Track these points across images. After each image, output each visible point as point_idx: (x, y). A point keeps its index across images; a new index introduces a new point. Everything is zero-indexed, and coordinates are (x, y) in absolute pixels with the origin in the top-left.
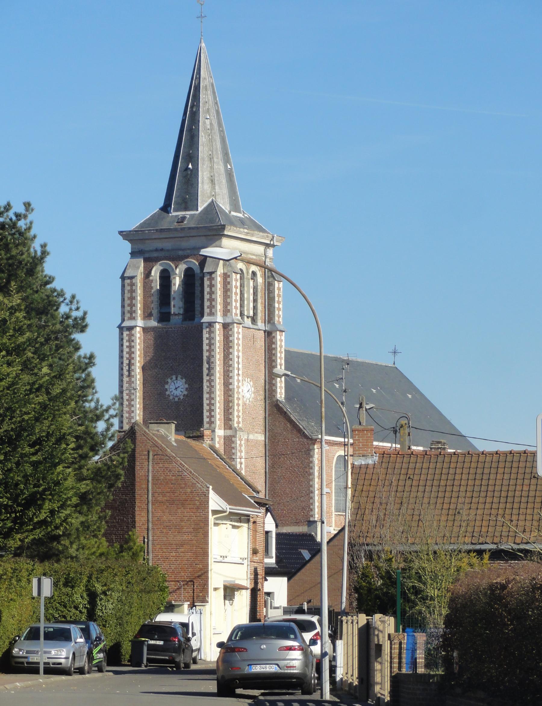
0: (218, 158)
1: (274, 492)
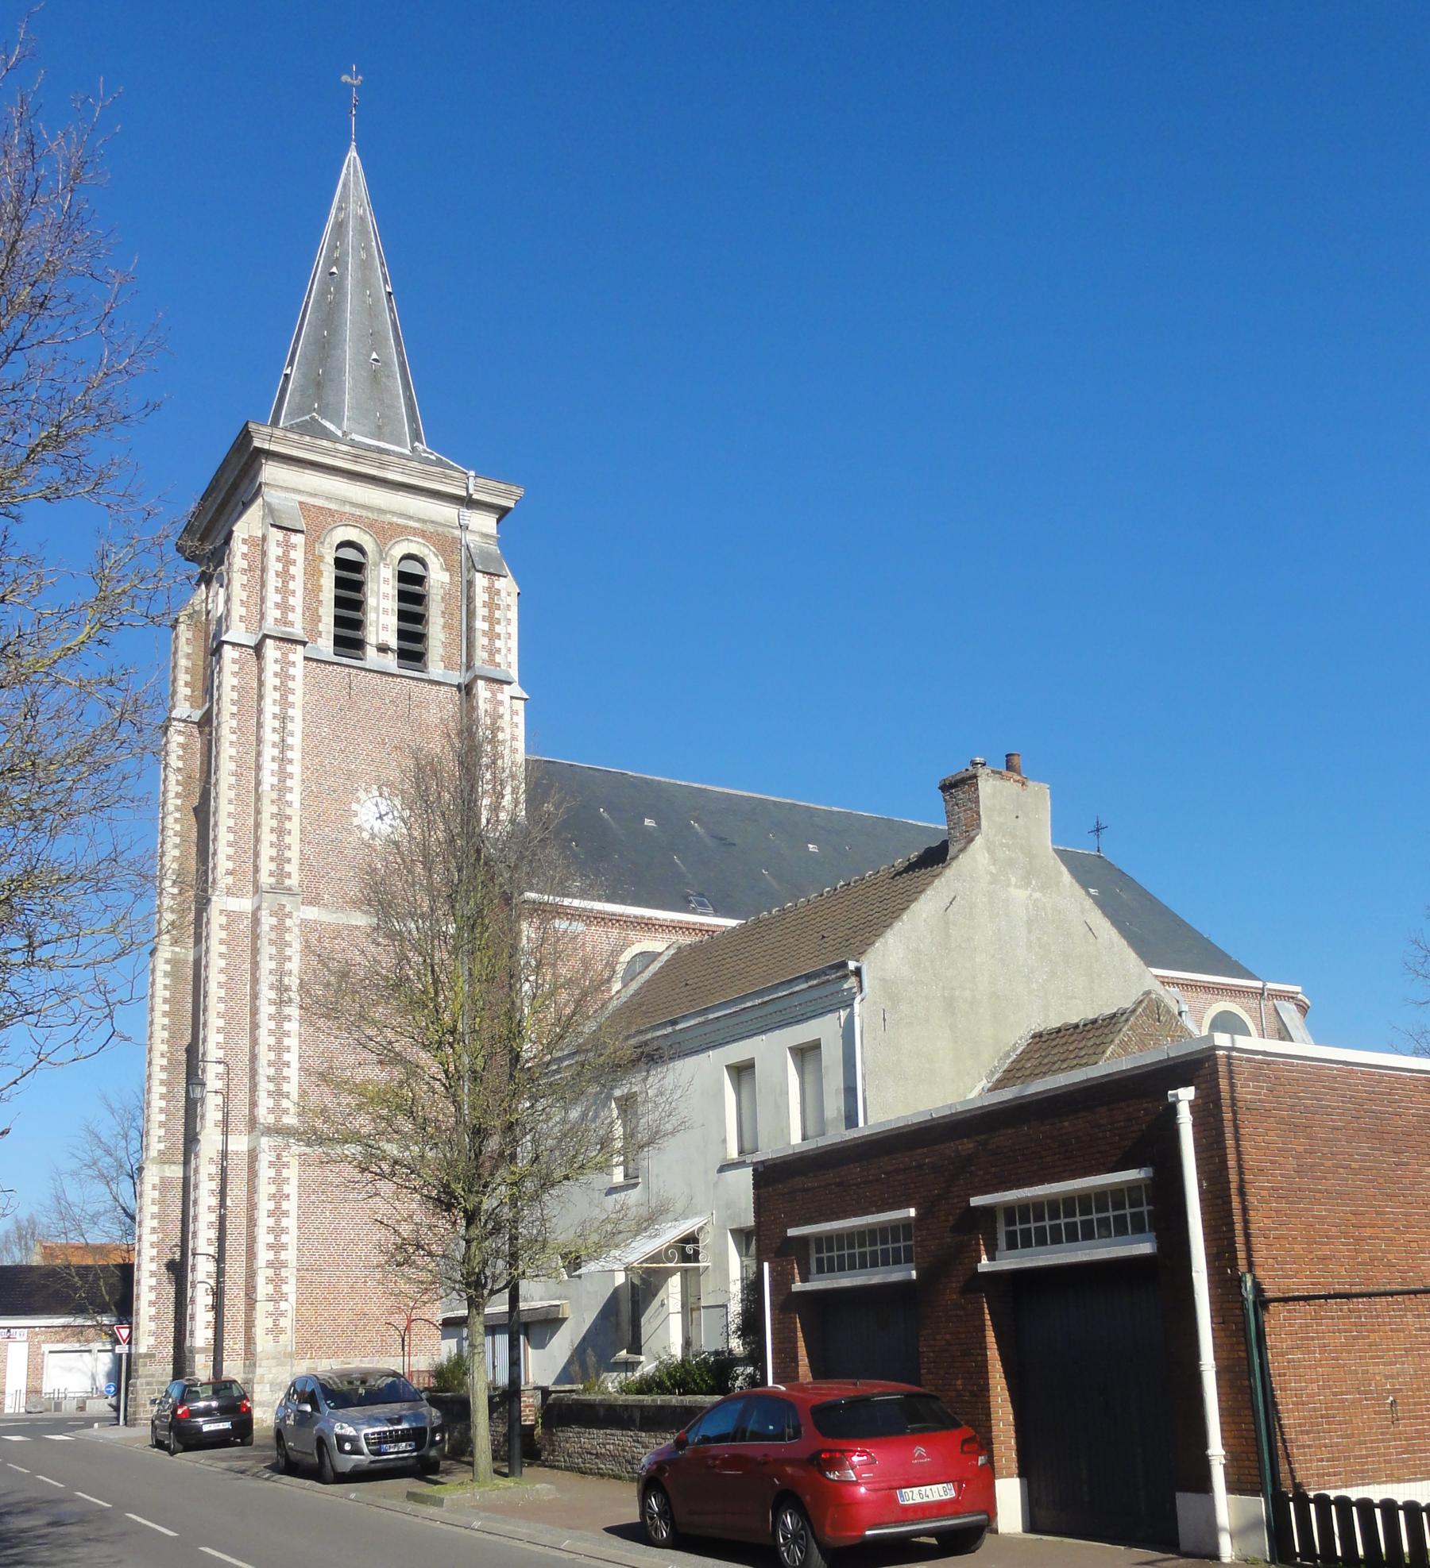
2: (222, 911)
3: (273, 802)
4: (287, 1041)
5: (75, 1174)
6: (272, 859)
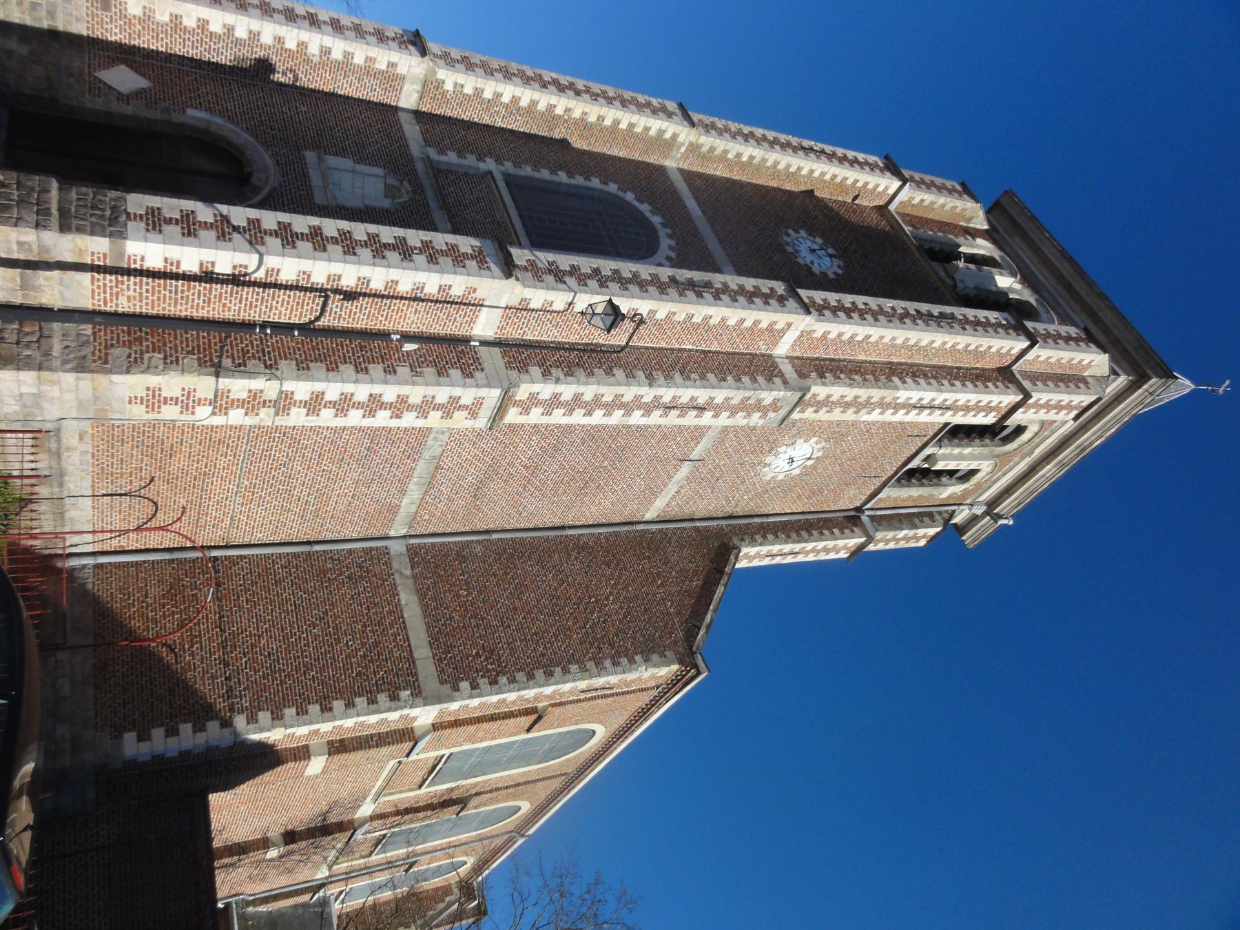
0: (471, 304)
1: (512, 555)
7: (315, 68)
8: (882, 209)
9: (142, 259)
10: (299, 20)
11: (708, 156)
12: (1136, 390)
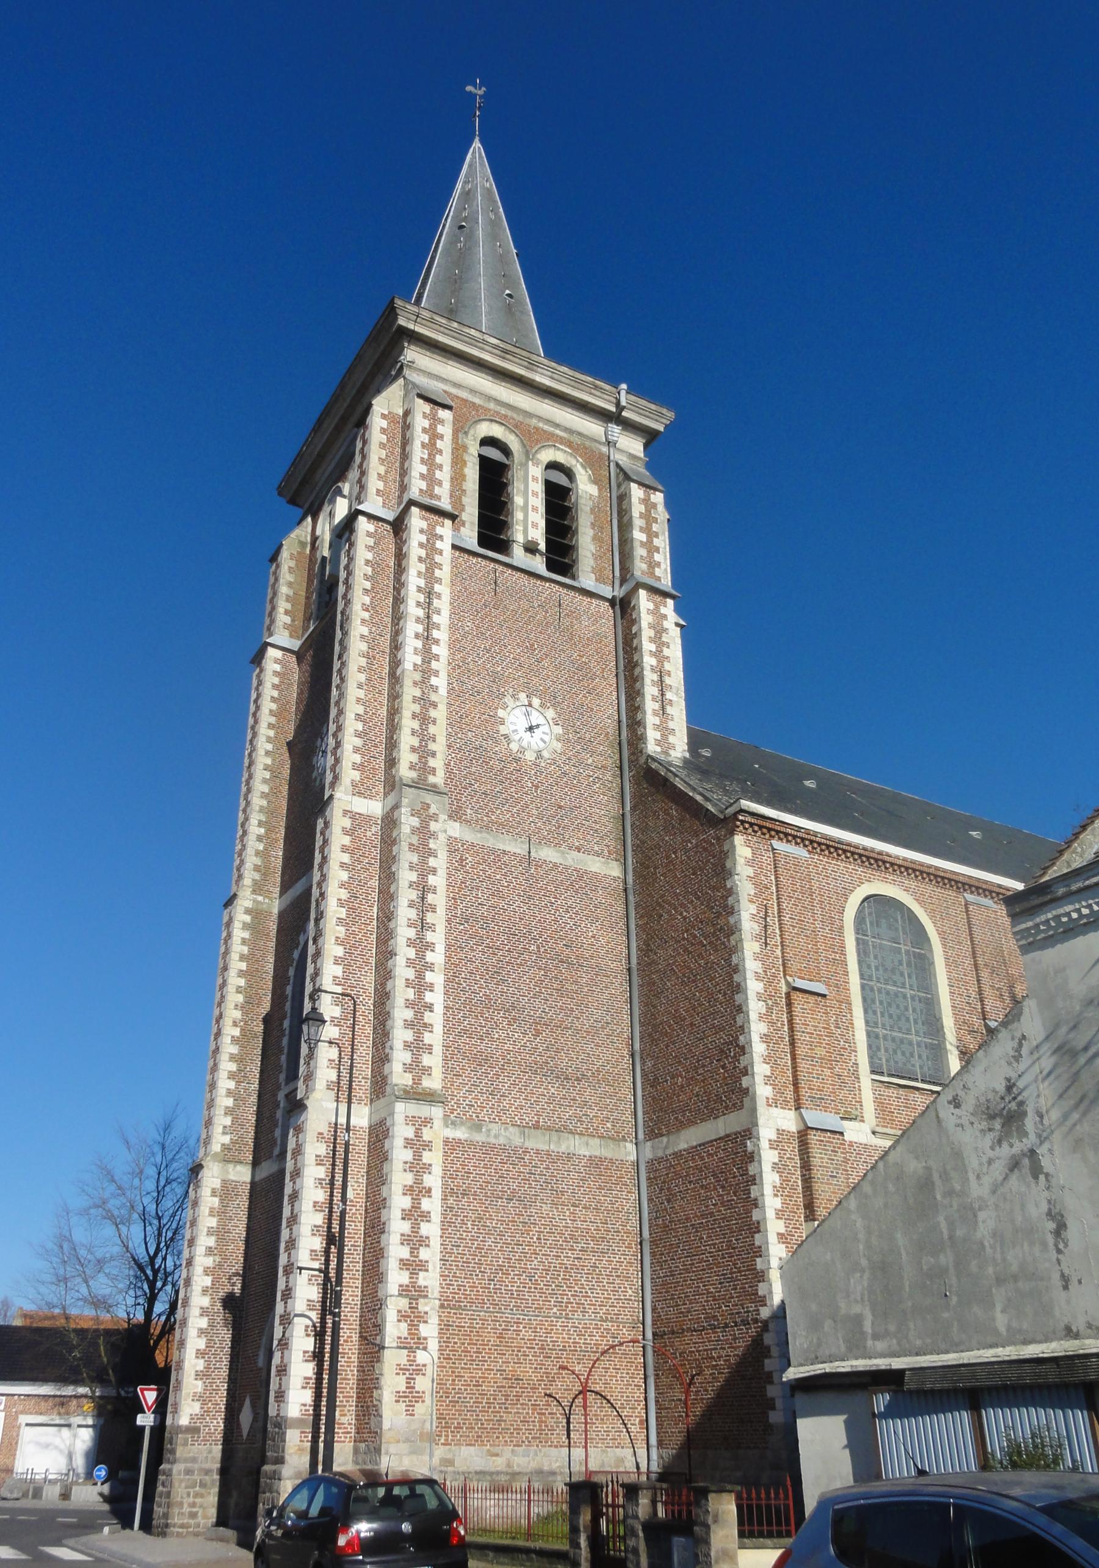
1: (654, 1026)
2: (346, 812)
3: (415, 683)
4: (429, 977)
5: (85, 1212)
6: (413, 749)
7: (225, 1259)
8: (299, 655)
9: (305, 1405)
10: (294, 1236)
11: (263, 870)
12: (418, 333)
